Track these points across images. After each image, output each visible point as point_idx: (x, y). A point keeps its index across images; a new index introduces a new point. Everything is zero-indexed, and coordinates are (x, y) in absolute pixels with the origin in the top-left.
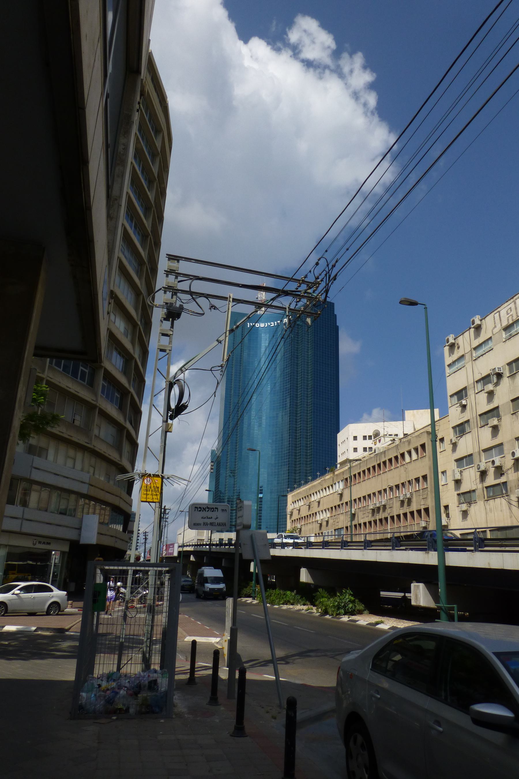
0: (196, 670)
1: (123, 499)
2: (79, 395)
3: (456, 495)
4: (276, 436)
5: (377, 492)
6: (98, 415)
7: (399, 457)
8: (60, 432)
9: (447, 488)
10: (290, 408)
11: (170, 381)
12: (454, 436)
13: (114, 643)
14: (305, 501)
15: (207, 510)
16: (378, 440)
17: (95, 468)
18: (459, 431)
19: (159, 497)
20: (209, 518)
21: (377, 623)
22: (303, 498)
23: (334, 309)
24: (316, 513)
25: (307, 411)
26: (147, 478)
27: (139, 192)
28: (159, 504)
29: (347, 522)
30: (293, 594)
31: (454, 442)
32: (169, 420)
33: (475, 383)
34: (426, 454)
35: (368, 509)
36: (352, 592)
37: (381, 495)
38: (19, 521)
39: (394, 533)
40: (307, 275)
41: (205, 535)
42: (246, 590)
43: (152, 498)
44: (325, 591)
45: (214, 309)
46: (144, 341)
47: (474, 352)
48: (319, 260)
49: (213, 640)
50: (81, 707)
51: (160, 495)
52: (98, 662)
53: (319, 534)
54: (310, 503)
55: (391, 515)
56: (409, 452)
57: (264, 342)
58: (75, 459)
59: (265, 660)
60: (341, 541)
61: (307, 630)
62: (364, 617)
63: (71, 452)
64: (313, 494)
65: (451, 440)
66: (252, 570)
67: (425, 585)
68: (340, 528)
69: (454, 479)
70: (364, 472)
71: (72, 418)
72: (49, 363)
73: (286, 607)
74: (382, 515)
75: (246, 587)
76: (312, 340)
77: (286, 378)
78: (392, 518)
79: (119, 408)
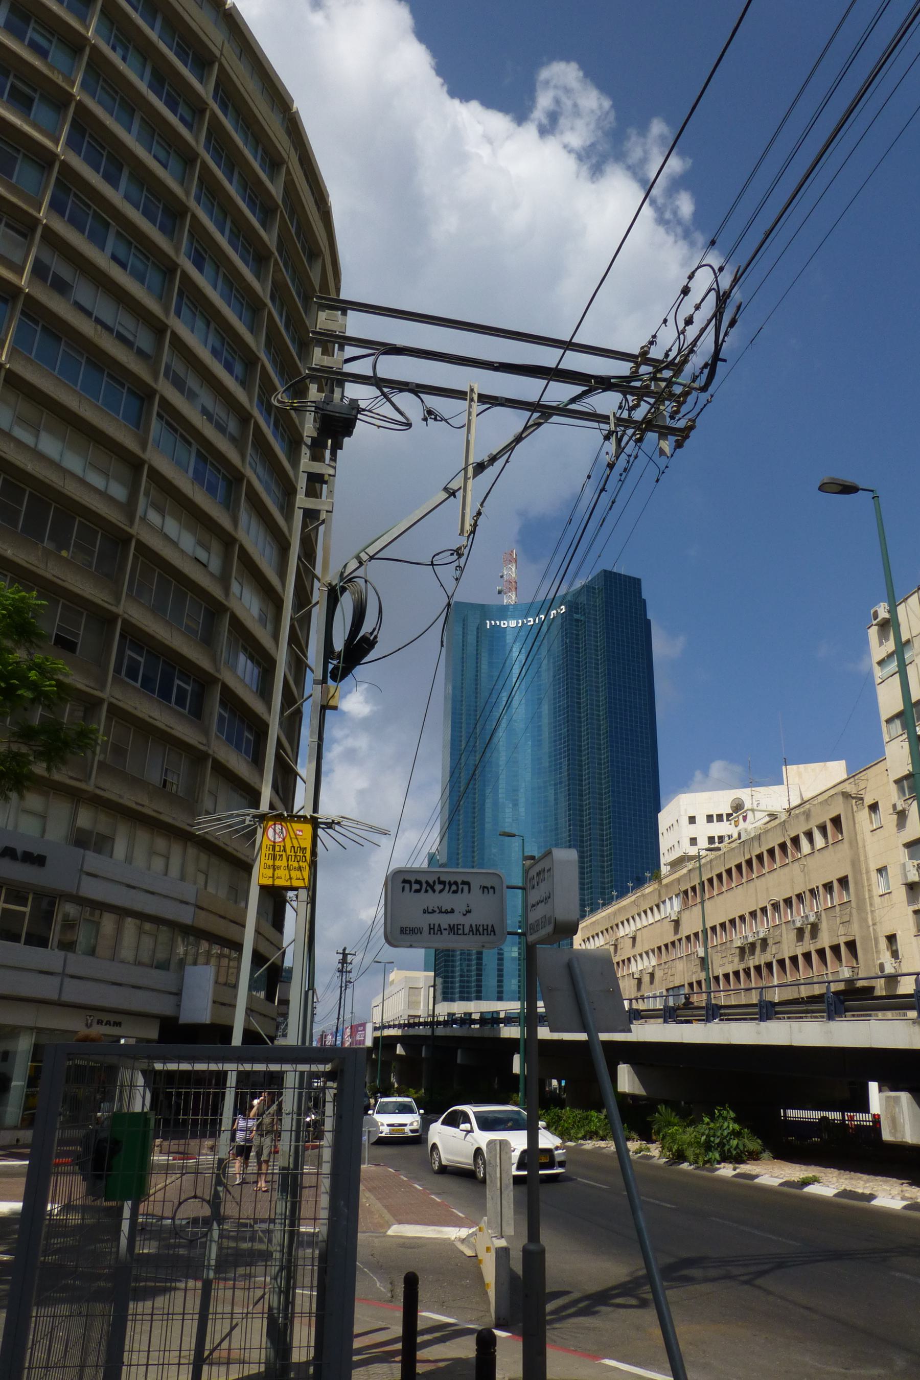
0: (419, 1339)
2: (173, 732)
3: (912, 913)
5: (747, 914)
7: (789, 844)
8: (137, 803)
9: (891, 901)
11: (330, 584)
12: (899, 798)
14: (608, 937)
15: (438, 887)
16: (741, 817)
17: (207, 875)
18: (909, 788)
19: (306, 874)
20: (446, 912)
21: (805, 1183)
22: (602, 932)
24: (629, 959)
25: (601, 774)
26: (275, 824)
27: (281, 361)
28: (308, 891)
29: (690, 973)
30: (602, 1117)
32: (330, 681)
34: (842, 836)
35: (730, 948)
37: (745, 923)
38: (56, 980)
39: (829, 982)
40: (654, 337)
41: (422, 1008)
45: (435, 419)
48: (691, 277)
49: (453, 1233)
51: (310, 868)
54: (617, 940)
55: (779, 957)
56: (809, 835)
57: (516, 654)
62: (766, 1167)
63: (161, 844)
64: (622, 923)
65: (894, 806)
66: (516, 1069)
69: (905, 882)
70: (720, 876)
72: (114, 671)
73: (590, 1145)
74: (759, 959)
77: (560, 716)
78: (781, 963)
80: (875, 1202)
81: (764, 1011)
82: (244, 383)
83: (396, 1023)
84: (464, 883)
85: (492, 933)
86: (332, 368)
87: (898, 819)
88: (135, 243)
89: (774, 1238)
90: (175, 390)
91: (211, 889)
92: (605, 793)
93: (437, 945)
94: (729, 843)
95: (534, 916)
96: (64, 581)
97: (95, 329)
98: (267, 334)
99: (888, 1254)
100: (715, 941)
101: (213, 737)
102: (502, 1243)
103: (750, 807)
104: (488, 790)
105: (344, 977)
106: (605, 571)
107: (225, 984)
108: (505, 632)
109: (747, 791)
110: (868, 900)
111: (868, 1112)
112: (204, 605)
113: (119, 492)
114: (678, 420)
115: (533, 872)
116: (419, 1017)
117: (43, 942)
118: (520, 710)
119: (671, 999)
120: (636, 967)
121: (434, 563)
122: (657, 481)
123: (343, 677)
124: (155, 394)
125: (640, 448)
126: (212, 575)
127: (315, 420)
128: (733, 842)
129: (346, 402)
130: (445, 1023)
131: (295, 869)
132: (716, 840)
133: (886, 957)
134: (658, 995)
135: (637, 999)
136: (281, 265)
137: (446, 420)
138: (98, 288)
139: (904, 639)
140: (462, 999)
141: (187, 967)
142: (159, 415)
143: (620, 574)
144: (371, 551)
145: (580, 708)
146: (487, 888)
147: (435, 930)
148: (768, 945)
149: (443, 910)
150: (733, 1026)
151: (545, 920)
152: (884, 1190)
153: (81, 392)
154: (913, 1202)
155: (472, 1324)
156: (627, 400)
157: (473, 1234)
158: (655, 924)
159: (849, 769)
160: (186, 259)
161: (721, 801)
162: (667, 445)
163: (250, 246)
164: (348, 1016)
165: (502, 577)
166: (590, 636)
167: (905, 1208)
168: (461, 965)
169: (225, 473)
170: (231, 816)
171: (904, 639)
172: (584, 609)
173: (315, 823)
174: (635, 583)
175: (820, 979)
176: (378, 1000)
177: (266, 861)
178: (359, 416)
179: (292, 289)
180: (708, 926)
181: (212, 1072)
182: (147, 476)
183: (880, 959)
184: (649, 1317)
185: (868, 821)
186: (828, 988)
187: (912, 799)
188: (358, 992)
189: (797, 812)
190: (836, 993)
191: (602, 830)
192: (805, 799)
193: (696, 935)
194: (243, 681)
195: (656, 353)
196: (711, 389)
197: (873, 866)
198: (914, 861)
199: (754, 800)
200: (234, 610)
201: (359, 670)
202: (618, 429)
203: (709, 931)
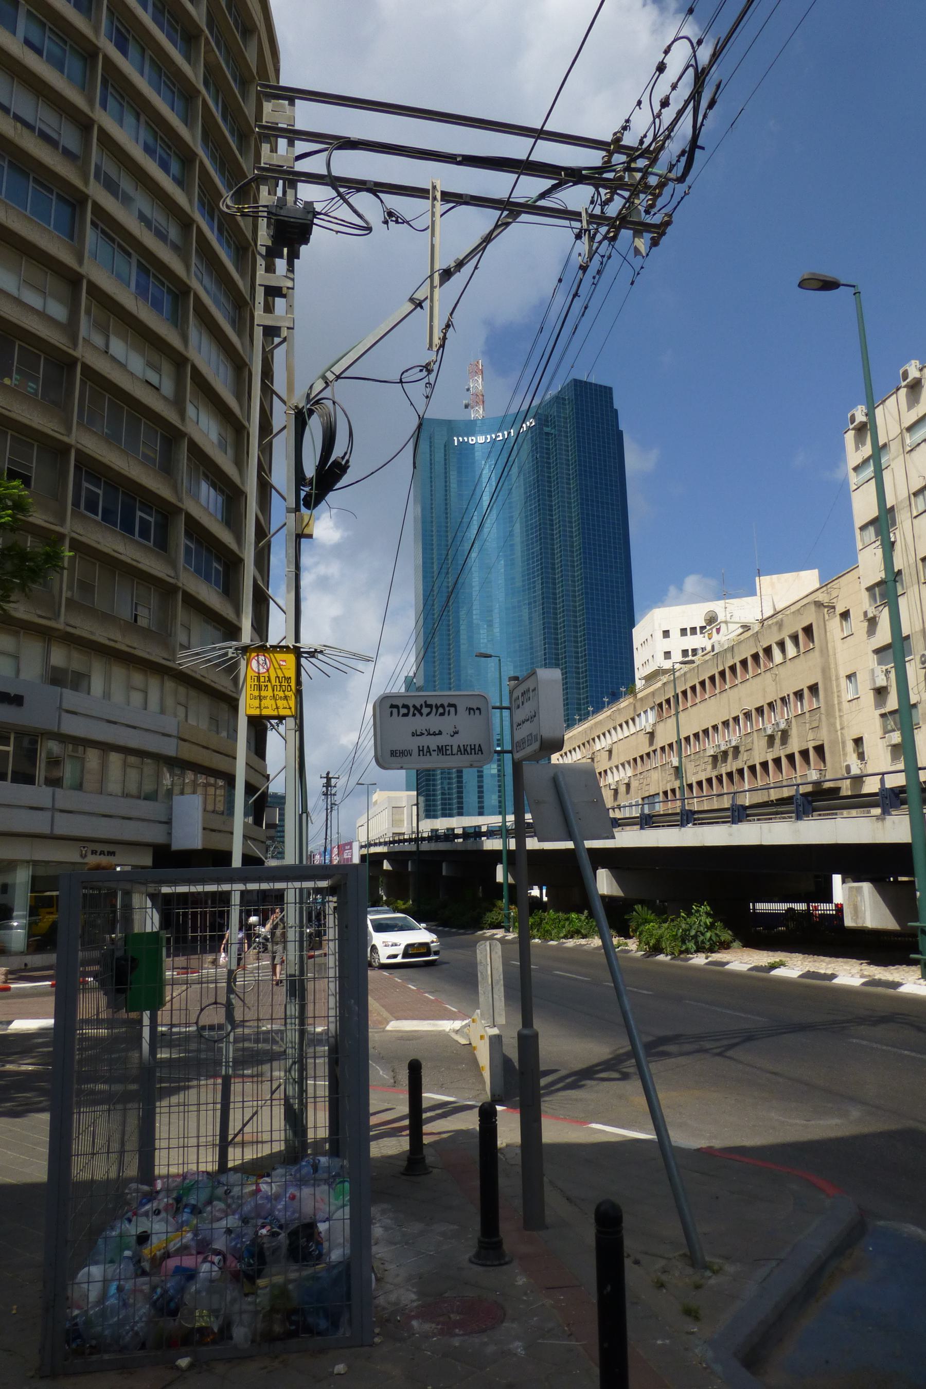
0: (425, 1116)
2: (140, 566)
4: (521, 641)
5: (720, 724)
6: (182, 606)
7: (761, 654)
8: (109, 639)
11: (296, 407)
12: (870, 606)
15: (425, 710)
16: (714, 630)
17: (186, 708)
18: (880, 594)
19: (292, 703)
20: (434, 734)
21: (773, 967)
22: (579, 747)
23: (611, 398)
24: (605, 771)
26: (258, 656)
28: (296, 719)
29: (665, 782)
30: (583, 918)
31: (872, 615)
32: (303, 508)
33: (912, 497)
37: (717, 733)
39: (798, 785)
40: (628, 121)
42: (491, 917)
43: (274, 707)
44: (649, 909)
45: (397, 222)
47: (907, 436)
49: (447, 1026)
50: (75, 1334)
51: (296, 698)
52: (165, 1135)
53: (765, 765)
54: (593, 753)
55: (750, 763)
61: (635, 990)
63: (138, 678)
64: (599, 737)
65: (865, 613)
66: (500, 878)
68: (653, 796)
69: (873, 687)
70: (693, 688)
71: (132, 600)
74: (732, 765)
75: (491, 911)
76: (575, 461)
77: (532, 534)
78: (752, 769)
80: (835, 981)
81: (736, 814)
82: (180, 182)
83: (382, 840)
84: (450, 705)
85: (480, 752)
86: (283, 166)
88: (48, 24)
89: (743, 1015)
90: (109, 194)
91: (192, 721)
92: (580, 611)
93: (419, 766)
94: (703, 656)
95: (521, 734)
96: (10, 411)
97: (15, 128)
98: (203, 126)
99: (848, 1024)
100: (688, 750)
101: (181, 570)
102: (495, 1031)
103: (724, 619)
104: (463, 613)
105: (329, 800)
106: (575, 381)
107: (213, 812)
108: (473, 449)
109: (721, 603)
110: (837, 706)
111: (832, 903)
112: (160, 431)
113: (58, 311)
114: (654, 214)
115: (517, 693)
116: (404, 834)
117: (29, 779)
118: (492, 531)
119: (646, 807)
120: (612, 779)
121: (403, 380)
122: (632, 283)
123: (317, 503)
124: (87, 200)
125: (613, 247)
126: (165, 398)
127: (268, 227)
128: (706, 654)
129: (300, 205)
130: (429, 839)
131: (281, 697)
132: (690, 653)
133: (852, 760)
134: (634, 803)
135: (613, 809)
136: (213, 44)
137: (408, 223)
138: (13, 78)
139: (881, 443)
140: (444, 815)
141: (174, 797)
142: (93, 223)
143: (591, 384)
144: (337, 369)
145: (552, 525)
146: (473, 709)
147: (424, 751)
148: (740, 752)
149: (431, 733)
150: (706, 829)
151: (531, 738)
152: (845, 970)
153: (5, 200)
154: (871, 979)
155: (470, 1101)
156: (599, 193)
157: (468, 1025)
158: (630, 737)
160: (108, 42)
161: (695, 615)
162: (641, 244)
163: (177, 23)
164: (335, 836)
165: (468, 390)
166: (560, 449)
167: (864, 984)
168: (442, 783)
169: (170, 286)
170: (214, 649)
171: (881, 443)
172: (555, 422)
173: (298, 652)
174: (606, 392)
175: (789, 783)
176: (362, 820)
177: (252, 692)
178: (316, 221)
179: (227, 73)
180: (682, 736)
181: (207, 893)
182: (87, 293)
183: (846, 761)
184: (633, 1088)
186: (797, 790)
187: (883, 606)
188: (343, 813)
189: (770, 622)
190: (805, 795)
191: (577, 647)
192: (778, 610)
193: (671, 745)
194: (206, 509)
195: (629, 140)
196: (689, 179)
197: (843, 673)
199: (727, 612)
200: (192, 436)
201: (331, 497)
202: (591, 227)
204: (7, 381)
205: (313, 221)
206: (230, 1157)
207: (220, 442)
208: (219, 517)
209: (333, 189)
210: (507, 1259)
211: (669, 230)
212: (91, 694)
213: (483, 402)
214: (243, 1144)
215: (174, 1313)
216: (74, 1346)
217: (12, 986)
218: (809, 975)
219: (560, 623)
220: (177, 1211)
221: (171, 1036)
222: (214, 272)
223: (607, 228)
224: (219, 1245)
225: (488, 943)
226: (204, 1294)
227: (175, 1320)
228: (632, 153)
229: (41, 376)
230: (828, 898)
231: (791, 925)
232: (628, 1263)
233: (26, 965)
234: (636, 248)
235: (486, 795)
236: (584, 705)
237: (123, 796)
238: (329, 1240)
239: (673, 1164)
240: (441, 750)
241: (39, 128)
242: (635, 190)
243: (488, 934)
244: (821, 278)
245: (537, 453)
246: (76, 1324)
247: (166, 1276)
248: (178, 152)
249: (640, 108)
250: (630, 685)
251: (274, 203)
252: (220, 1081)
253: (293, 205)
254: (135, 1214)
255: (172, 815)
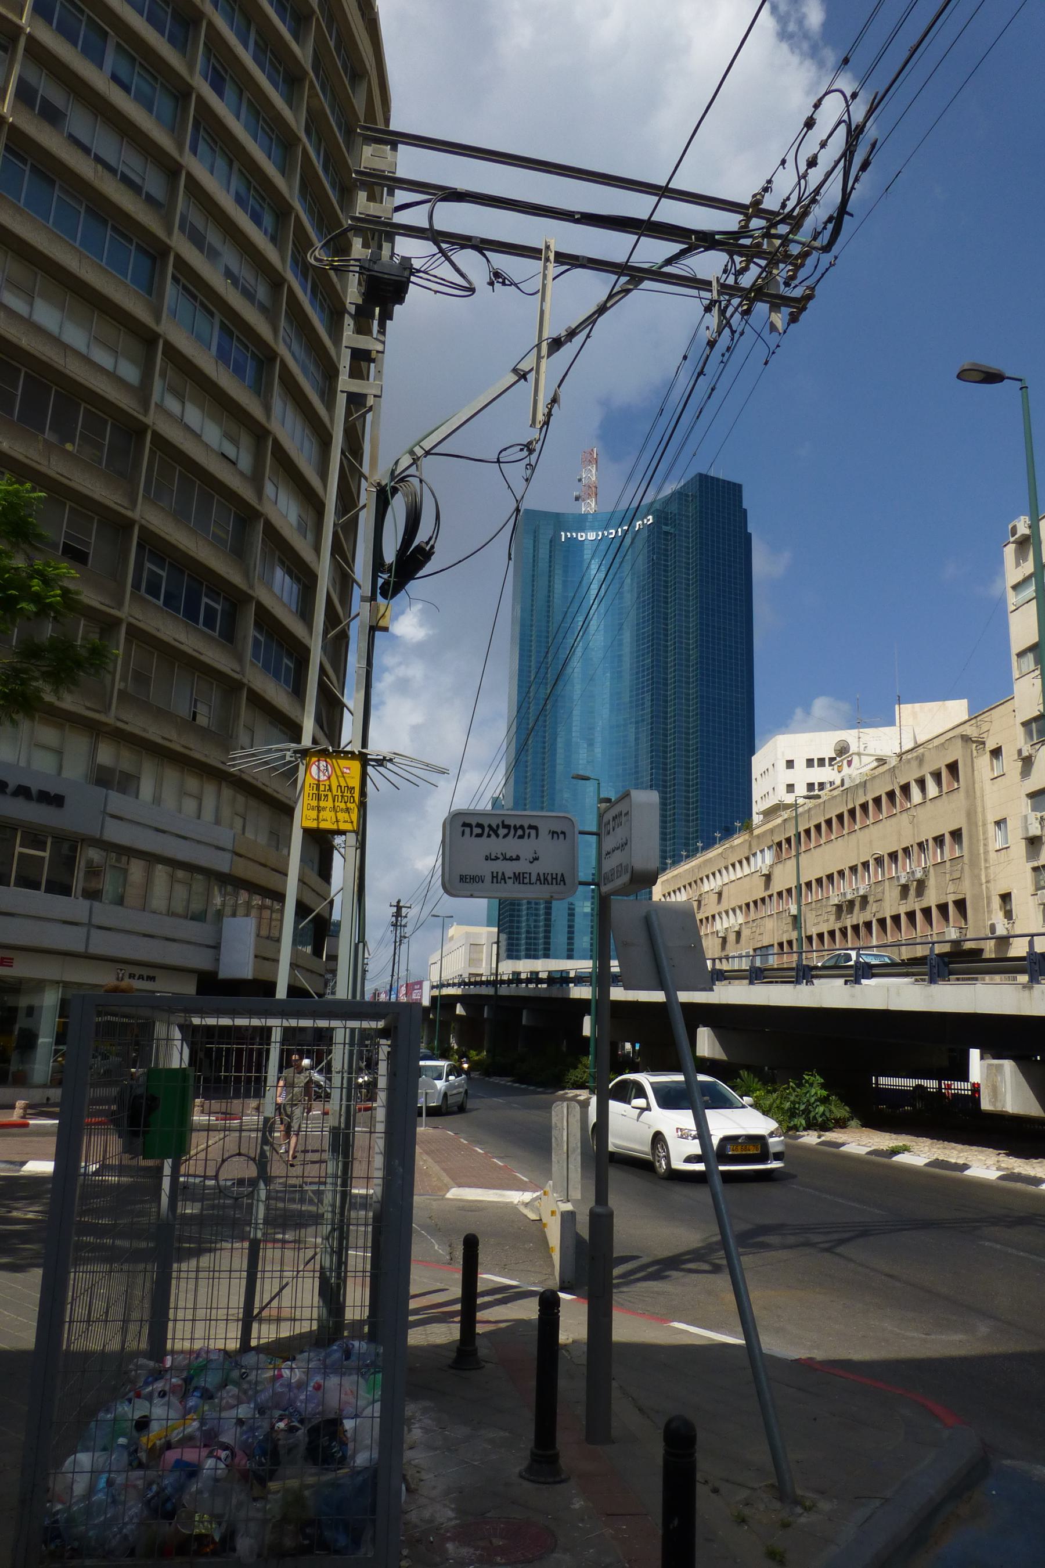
0: (479, 1301)
1: (310, 887)
3: (1030, 870)
5: (847, 869)
7: (898, 792)
8: (164, 738)
10: (652, 706)
11: (379, 484)
12: (1026, 743)
13: (281, 1205)
15: (502, 832)
16: (845, 762)
17: (245, 819)
18: (1038, 731)
19: (354, 816)
20: (511, 859)
21: (894, 1152)
22: (685, 887)
23: (741, 497)
24: (713, 917)
25: (688, 711)
26: (319, 761)
27: (318, 211)
28: (357, 834)
29: (781, 932)
31: (1027, 754)
32: (379, 597)
36: (821, 1077)
37: (822, 887)
39: (933, 943)
40: (769, 182)
42: (574, 1075)
43: (334, 819)
45: (504, 284)
46: (344, 550)
48: (817, 106)
49: (516, 1197)
50: (54, 1533)
53: (896, 919)
54: (701, 895)
55: (879, 916)
56: (921, 783)
58: (201, 800)
59: (657, 1258)
60: (794, 965)
63: (192, 783)
64: (707, 877)
65: (1020, 752)
66: (587, 1031)
67: (1017, 1064)
68: (767, 947)
69: (1025, 836)
70: (818, 827)
71: (190, 708)
72: (132, 587)
74: (858, 917)
75: (576, 1068)
76: (696, 566)
78: (882, 922)
79: (293, 691)
80: (967, 1173)
83: (456, 981)
84: (531, 827)
85: (562, 883)
86: (380, 217)
87: (1023, 766)
88: (139, 59)
91: (250, 835)
94: (831, 791)
95: (608, 865)
96: (70, 480)
97: (96, 171)
102: (568, 1207)
105: (398, 932)
106: (701, 475)
107: (268, 938)
109: (854, 732)
110: (982, 855)
112: (233, 509)
113: (130, 372)
114: (794, 287)
116: (481, 975)
117: (65, 890)
119: (758, 959)
121: (501, 460)
122: (766, 363)
123: (395, 592)
126: (242, 474)
127: (359, 283)
128: (835, 789)
131: (342, 810)
132: (816, 787)
134: (744, 954)
135: (720, 959)
137: (516, 285)
140: (528, 957)
141: (225, 919)
142: (174, 277)
143: (718, 480)
144: (427, 444)
146: (557, 833)
147: (498, 878)
149: (508, 857)
151: (621, 869)
152: (980, 1160)
154: (1009, 1172)
156: (733, 262)
157: (539, 1198)
159: (971, 709)
161: (824, 743)
162: (779, 319)
163: (280, 64)
165: (580, 480)
167: (1000, 1178)
168: (528, 920)
170: (270, 751)
172: (675, 520)
173: (364, 760)
174: (734, 491)
175: (924, 940)
176: (436, 957)
177: (310, 802)
178: (413, 279)
180: (803, 881)
183: (991, 919)
184: (722, 1283)
185: (989, 767)
186: (932, 950)
188: (414, 947)
189: (909, 756)
192: (919, 742)
193: (789, 891)
194: (280, 599)
195: (770, 203)
196: (835, 250)
197: (991, 818)
198: (1037, 813)
199: (861, 743)
201: (413, 586)
202: (722, 298)
203: (803, 886)
204: (69, 447)
205: (410, 278)
206: (254, 1334)
207: (299, 524)
208: (294, 608)
209: (435, 244)
210: (563, 1477)
211: (811, 305)
212: (140, 796)
213: (596, 495)
214: (279, 1320)
215: (170, 1515)
216: (52, 1547)
217: (31, 1122)
218: (936, 1163)
219: (670, 746)
220: (184, 1397)
221: (204, 1190)
222: (304, 337)
223: (740, 299)
224: (226, 1438)
225: (565, 1104)
226: (206, 1495)
227: (170, 1524)
228: (773, 218)
229: (107, 443)
230: (965, 1078)
231: (919, 1105)
232: (701, 1490)
233: (48, 1099)
234: (772, 324)
235: (576, 935)
236: (693, 839)
237: (168, 915)
238: (355, 1440)
239: (763, 1377)
240: (518, 878)
241: (122, 172)
242: (772, 259)
243: (570, 1095)
244: (983, 369)
245: (654, 554)
246: (56, 1522)
247: (163, 1471)
248: (272, 204)
249: (784, 168)
250: (747, 820)
251: (367, 256)
252: (246, 1244)
253: (388, 259)
254: (138, 1396)
255: (221, 939)
